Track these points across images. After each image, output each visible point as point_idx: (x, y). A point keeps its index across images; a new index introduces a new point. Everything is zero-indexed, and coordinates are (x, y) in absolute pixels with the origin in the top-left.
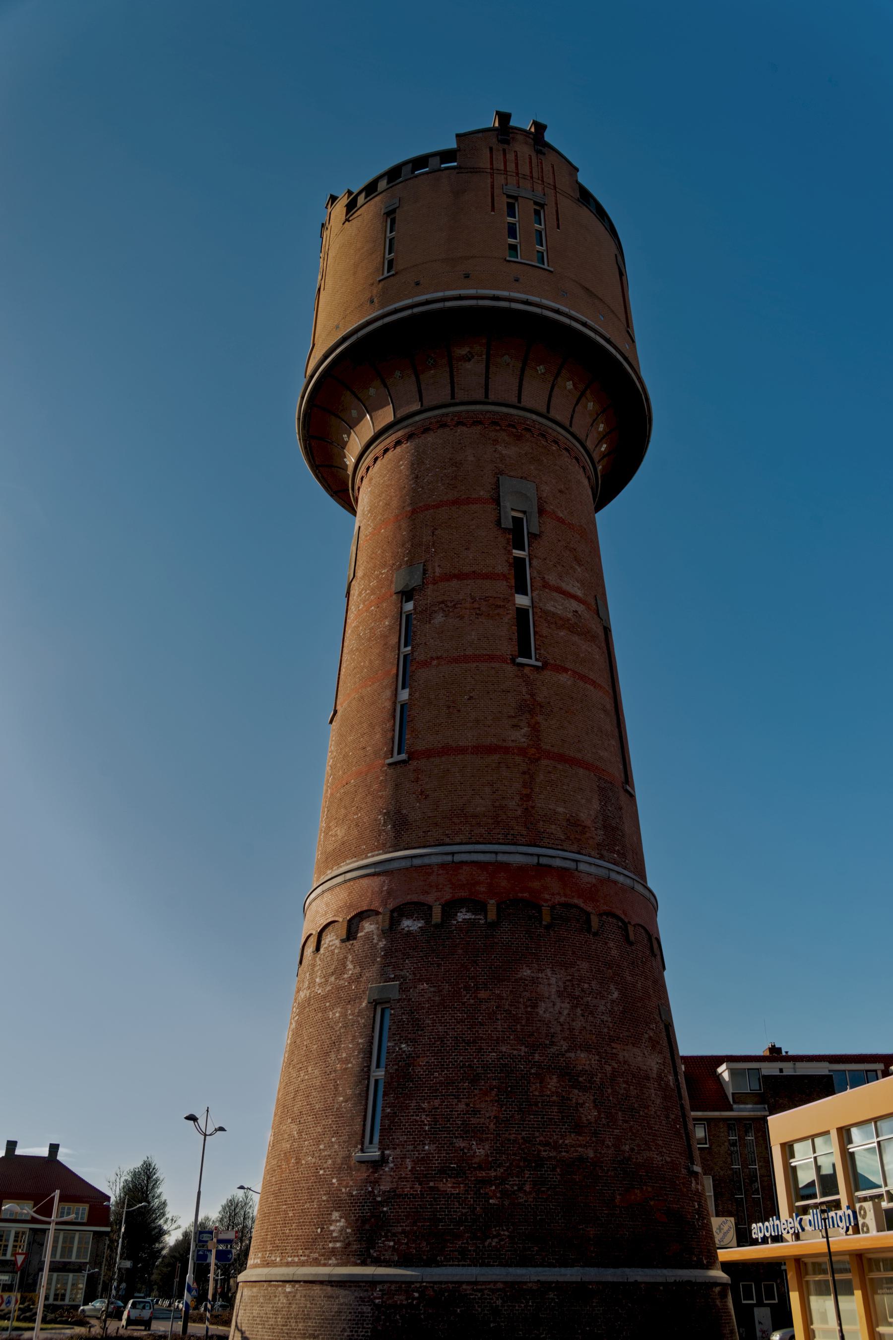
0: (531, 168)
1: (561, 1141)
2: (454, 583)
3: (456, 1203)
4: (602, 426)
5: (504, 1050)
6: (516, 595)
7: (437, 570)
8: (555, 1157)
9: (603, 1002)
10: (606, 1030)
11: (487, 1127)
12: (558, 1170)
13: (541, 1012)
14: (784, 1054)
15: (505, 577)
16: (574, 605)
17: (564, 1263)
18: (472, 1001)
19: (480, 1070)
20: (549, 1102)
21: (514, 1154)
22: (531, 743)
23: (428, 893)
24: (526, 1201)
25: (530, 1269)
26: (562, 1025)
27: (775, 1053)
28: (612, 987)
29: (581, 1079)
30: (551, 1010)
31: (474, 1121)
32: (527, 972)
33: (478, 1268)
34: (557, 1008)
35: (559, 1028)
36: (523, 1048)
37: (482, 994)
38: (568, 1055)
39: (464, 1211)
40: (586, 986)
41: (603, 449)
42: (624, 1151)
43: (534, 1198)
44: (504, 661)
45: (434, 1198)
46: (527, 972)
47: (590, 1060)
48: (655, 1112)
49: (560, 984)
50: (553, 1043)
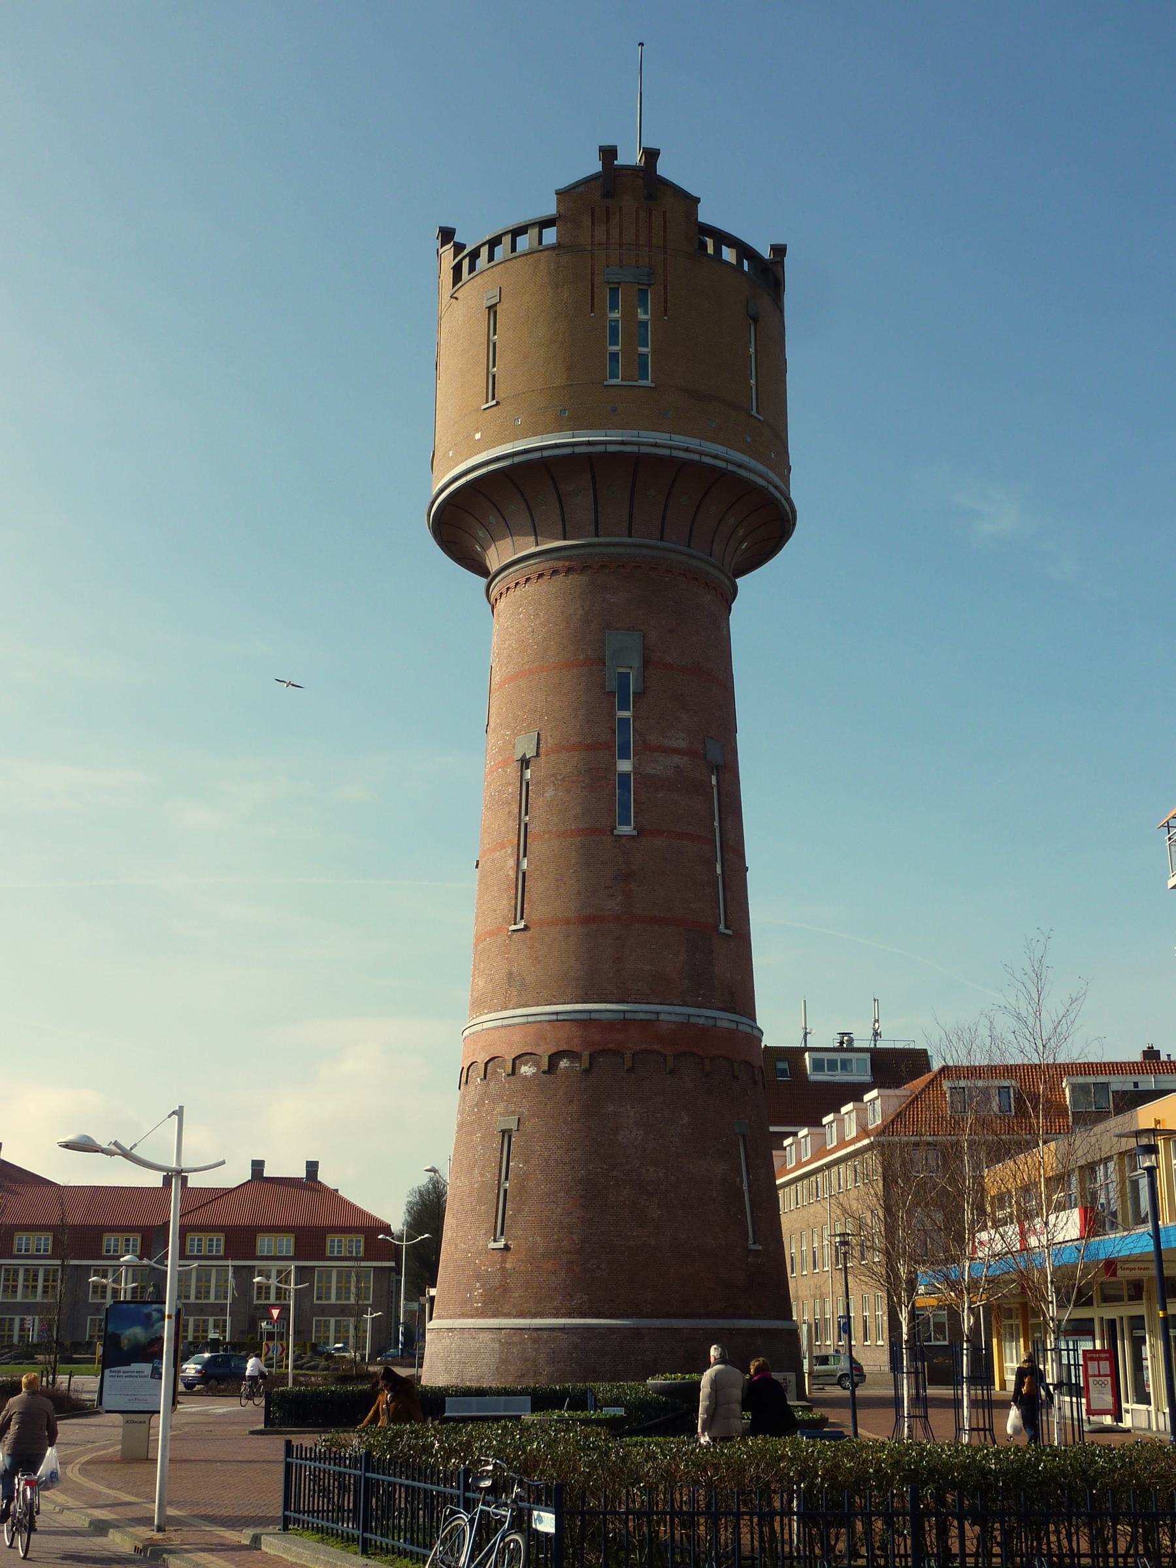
0: (637, 236)
14: (1163, 1058)
16: (676, 759)
32: (611, 1108)
46: (611, 1108)
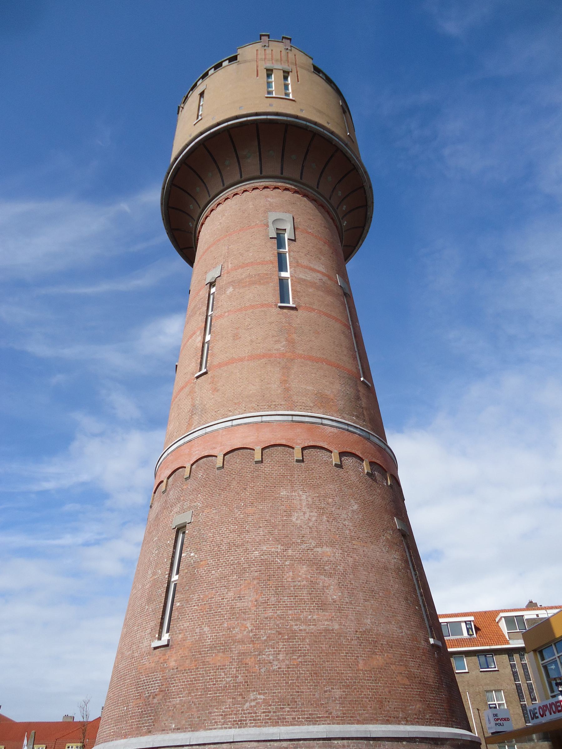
1: (309, 617)
2: (240, 271)
3: (223, 674)
4: (345, 207)
5: (265, 549)
6: (524, 645)
7: (230, 266)
8: (305, 630)
9: (345, 512)
10: (348, 532)
11: (250, 609)
12: (307, 640)
13: (294, 520)
15: (272, 262)
17: (312, 720)
18: (242, 516)
19: (246, 566)
20: (300, 586)
21: (271, 629)
22: (288, 350)
23: (215, 448)
24: (279, 668)
25: (282, 728)
26: (310, 528)
27: (532, 606)
28: (352, 501)
29: (326, 568)
30: (302, 518)
31: (239, 604)
32: (283, 493)
33: (238, 730)
34: (307, 516)
35: (308, 531)
36: (279, 546)
37: (250, 510)
38: (315, 550)
39: (228, 679)
40: (330, 500)
41: (344, 209)
42: (365, 624)
43: (286, 665)
44: (271, 306)
45: (205, 671)
46: (283, 493)
47: (335, 553)
48: (394, 595)
49: (309, 499)
50: (303, 542)
